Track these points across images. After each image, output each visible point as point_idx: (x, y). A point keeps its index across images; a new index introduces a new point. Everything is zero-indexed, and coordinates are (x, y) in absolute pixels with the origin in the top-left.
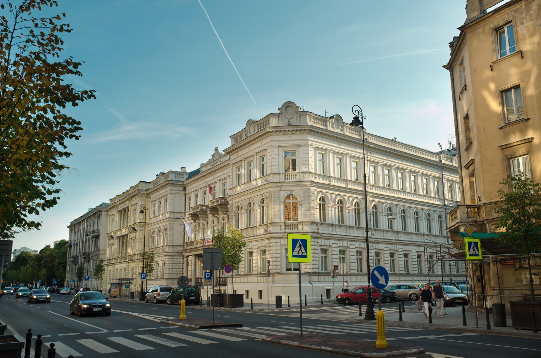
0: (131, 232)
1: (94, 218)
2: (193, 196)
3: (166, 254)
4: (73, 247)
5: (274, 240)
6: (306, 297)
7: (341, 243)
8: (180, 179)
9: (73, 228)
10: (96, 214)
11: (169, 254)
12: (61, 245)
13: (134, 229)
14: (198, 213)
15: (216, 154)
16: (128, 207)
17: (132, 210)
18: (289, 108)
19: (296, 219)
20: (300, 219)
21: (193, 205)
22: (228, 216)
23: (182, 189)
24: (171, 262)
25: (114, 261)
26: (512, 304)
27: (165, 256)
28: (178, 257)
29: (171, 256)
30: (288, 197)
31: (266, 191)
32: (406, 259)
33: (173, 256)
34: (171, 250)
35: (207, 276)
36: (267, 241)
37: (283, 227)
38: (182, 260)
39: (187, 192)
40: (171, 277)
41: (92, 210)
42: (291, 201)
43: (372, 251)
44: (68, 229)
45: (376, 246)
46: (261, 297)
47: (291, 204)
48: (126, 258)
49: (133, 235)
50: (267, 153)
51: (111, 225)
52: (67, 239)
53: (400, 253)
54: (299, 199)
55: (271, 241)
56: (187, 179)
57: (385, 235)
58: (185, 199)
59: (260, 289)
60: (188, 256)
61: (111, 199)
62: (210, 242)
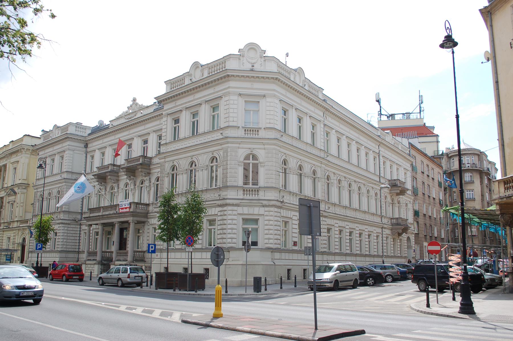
0: (9, 195)
3: (60, 221)
6: (295, 277)
8: (81, 134)
11: (63, 221)
13: (12, 190)
15: (134, 106)
19: (255, 183)
20: (262, 182)
21: (97, 163)
22: (150, 179)
23: (83, 145)
24: (66, 231)
26: (157, 274)
27: (59, 224)
28: (74, 226)
29: (66, 224)
30: (247, 158)
31: (220, 147)
33: (69, 224)
34: (66, 217)
35: (38, 247)
36: (220, 209)
37: (241, 192)
38: (79, 229)
39: (89, 150)
40: (65, 249)
42: (251, 161)
43: (324, 226)
45: (329, 221)
47: (251, 165)
49: (12, 198)
50: (222, 103)
54: (261, 160)
55: (225, 208)
56: (89, 134)
57: (336, 209)
58: (86, 157)
59: (289, 267)
60: (91, 225)
62: (126, 208)
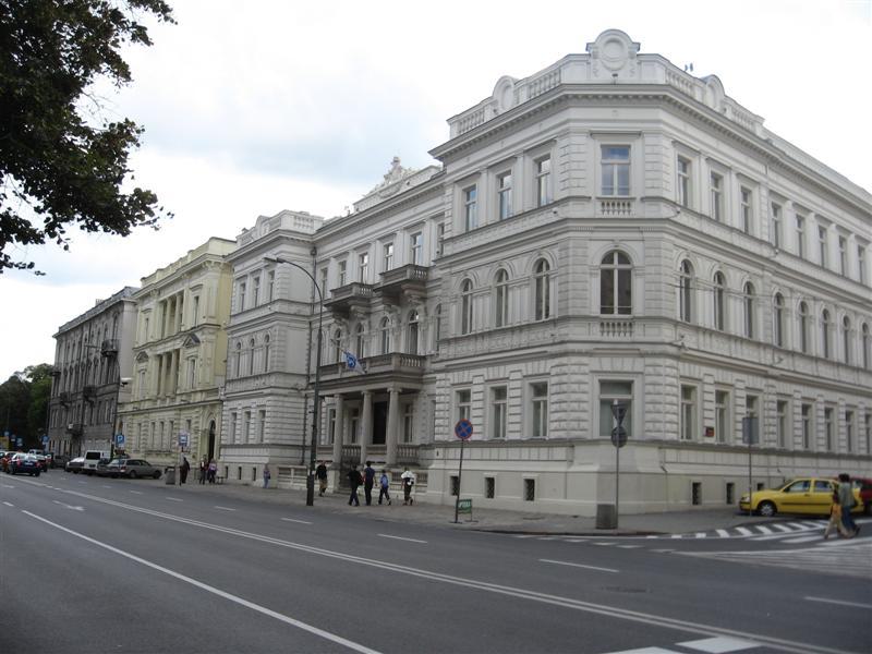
1: (108, 318)
2: (333, 267)
4: (62, 375)
5: (574, 359)
7: (492, 373)
9: (64, 339)
10: (111, 309)
12: (41, 372)
14: (350, 302)
16: (181, 293)
17: (192, 299)
18: (613, 45)
25: (147, 405)
30: (608, 259)
32: (687, 402)
38: (303, 406)
41: (100, 304)
44: (55, 341)
46: (491, 494)
48: (173, 399)
49: (192, 351)
51: (142, 328)
52: (51, 361)
53: (707, 388)
61: (143, 278)
